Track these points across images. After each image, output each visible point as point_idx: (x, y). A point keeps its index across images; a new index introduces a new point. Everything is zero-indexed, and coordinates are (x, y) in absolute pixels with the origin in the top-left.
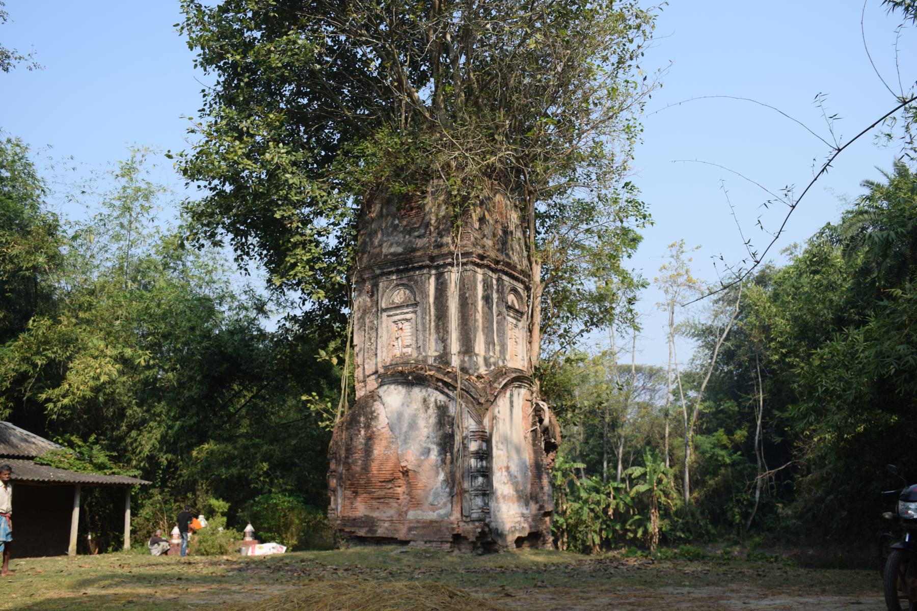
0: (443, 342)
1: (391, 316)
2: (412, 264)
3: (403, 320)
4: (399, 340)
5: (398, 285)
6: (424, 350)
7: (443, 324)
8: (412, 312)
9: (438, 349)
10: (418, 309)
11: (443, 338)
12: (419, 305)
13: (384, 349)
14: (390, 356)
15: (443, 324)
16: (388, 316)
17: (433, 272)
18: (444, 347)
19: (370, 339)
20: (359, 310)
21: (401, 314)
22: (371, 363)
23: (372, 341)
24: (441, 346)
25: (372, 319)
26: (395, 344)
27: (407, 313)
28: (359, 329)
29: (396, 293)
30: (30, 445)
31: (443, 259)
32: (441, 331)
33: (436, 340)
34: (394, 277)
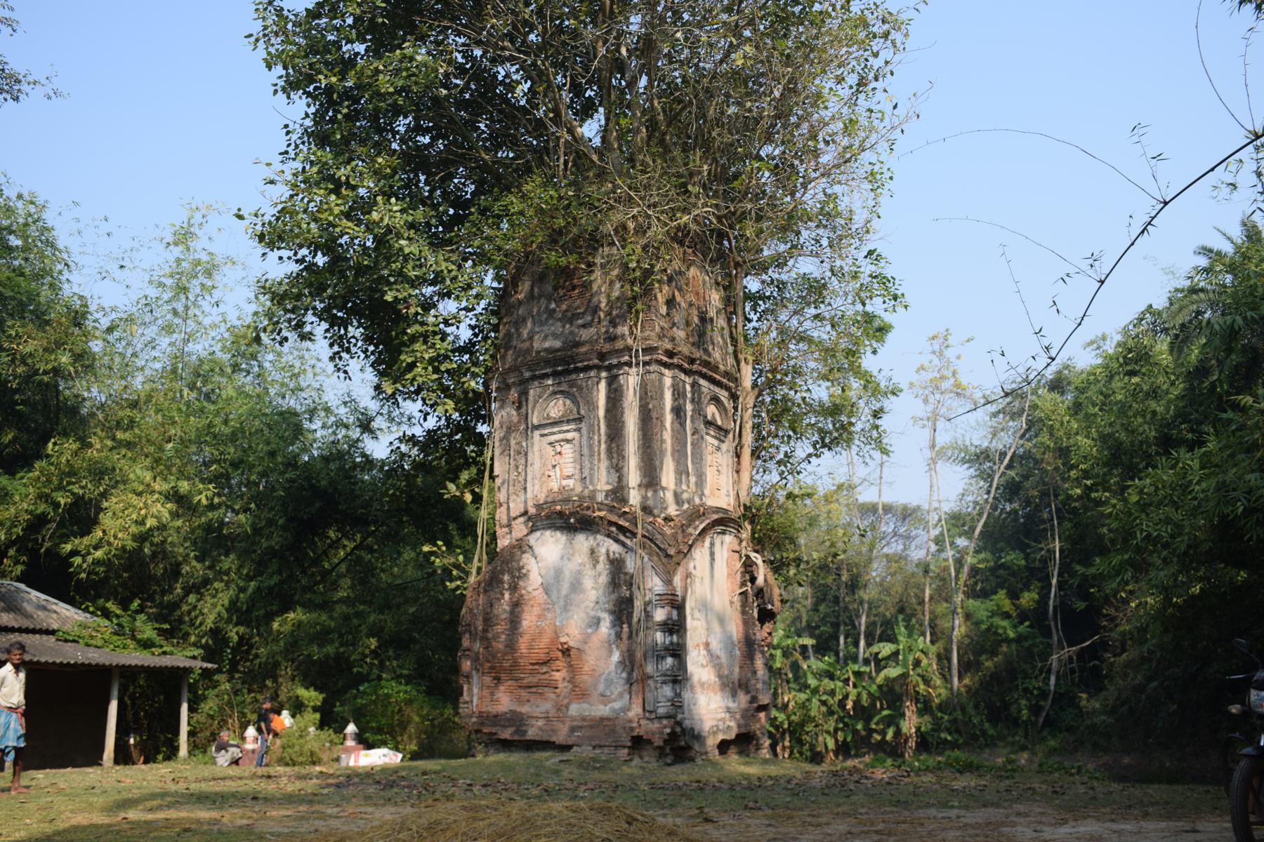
0: (617, 471)
1: (546, 435)
3: (563, 440)
5: (555, 393)
6: (591, 483)
7: (618, 446)
8: (575, 430)
9: (611, 481)
12: (585, 420)
13: (536, 482)
14: (545, 490)
15: (618, 446)
16: (542, 436)
17: (604, 374)
18: (619, 477)
19: (517, 467)
21: (560, 432)
22: (518, 500)
24: (615, 476)
25: (519, 440)
26: (552, 473)
27: (568, 431)
29: (552, 403)
31: (618, 357)
32: (615, 455)
33: (607, 468)
34: (550, 382)
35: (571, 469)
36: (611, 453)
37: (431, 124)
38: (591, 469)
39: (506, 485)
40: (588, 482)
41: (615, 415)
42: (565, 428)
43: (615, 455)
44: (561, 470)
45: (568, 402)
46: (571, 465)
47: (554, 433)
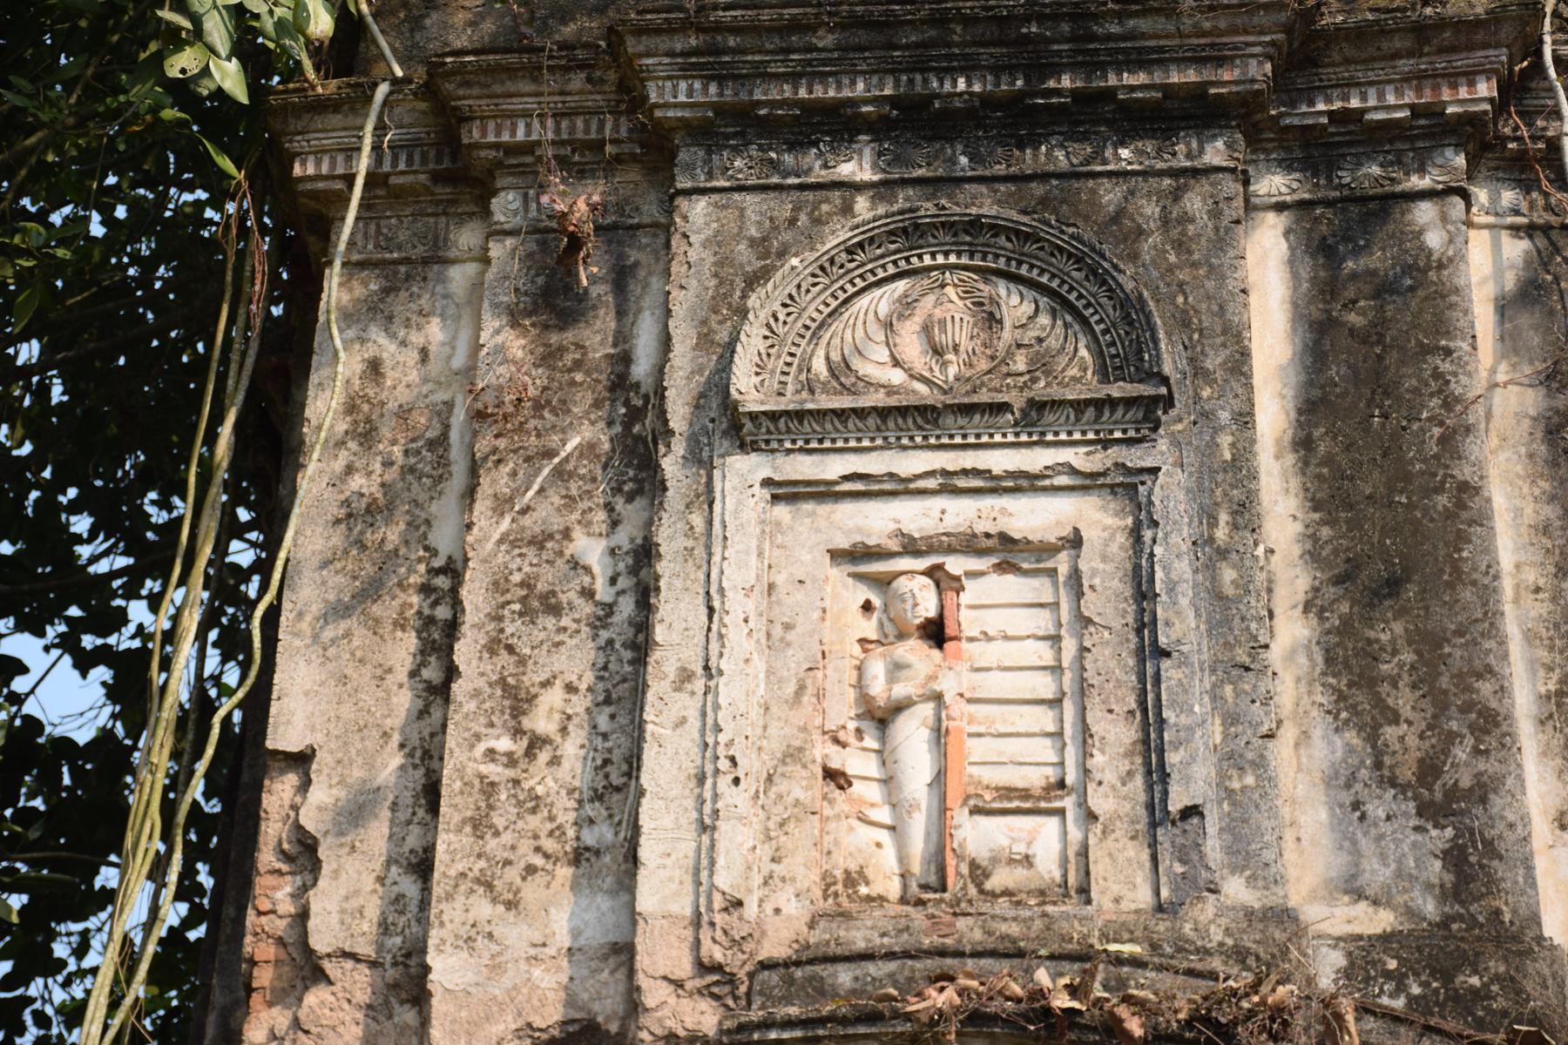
0: (1431, 813)
1: (825, 492)
2: (1093, 66)
3: (969, 544)
4: (912, 732)
5: (911, 233)
6: (1244, 857)
7: (1429, 644)
8: (1087, 483)
9: (1377, 874)
10: (1159, 453)
11: (1429, 770)
12: (1175, 423)
13: (734, 799)
14: (803, 870)
15: (1429, 644)
16: (785, 492)
17: (1273, 183)
18: (1454, 857)
19: (518, 701)
20: (366, 435)
21: (949, 484)
22: (515, 934)
23: (541, 721)
24: (1343, 859)
25: (547, 515)
26: (858, 762)
27: (1025, 483)
28: (339, 611)
29: (882, 300)
30: (466, 320)
31: (1417, 79)
32: (1404, 700)
33: (1341, 780)
34: (857, 167)
35: (1045, 750)
36: (1368, 680)
37: (48, 569)
38: (1232, 760)
39: (989, 484)
40: (1213, 848)
41: (1391, 449)
42: (1000, 461)
43: (1404, 700)
44: (939, 734)
45: (1015, 305)
46: (1045, 719)
47: (901, 488)
